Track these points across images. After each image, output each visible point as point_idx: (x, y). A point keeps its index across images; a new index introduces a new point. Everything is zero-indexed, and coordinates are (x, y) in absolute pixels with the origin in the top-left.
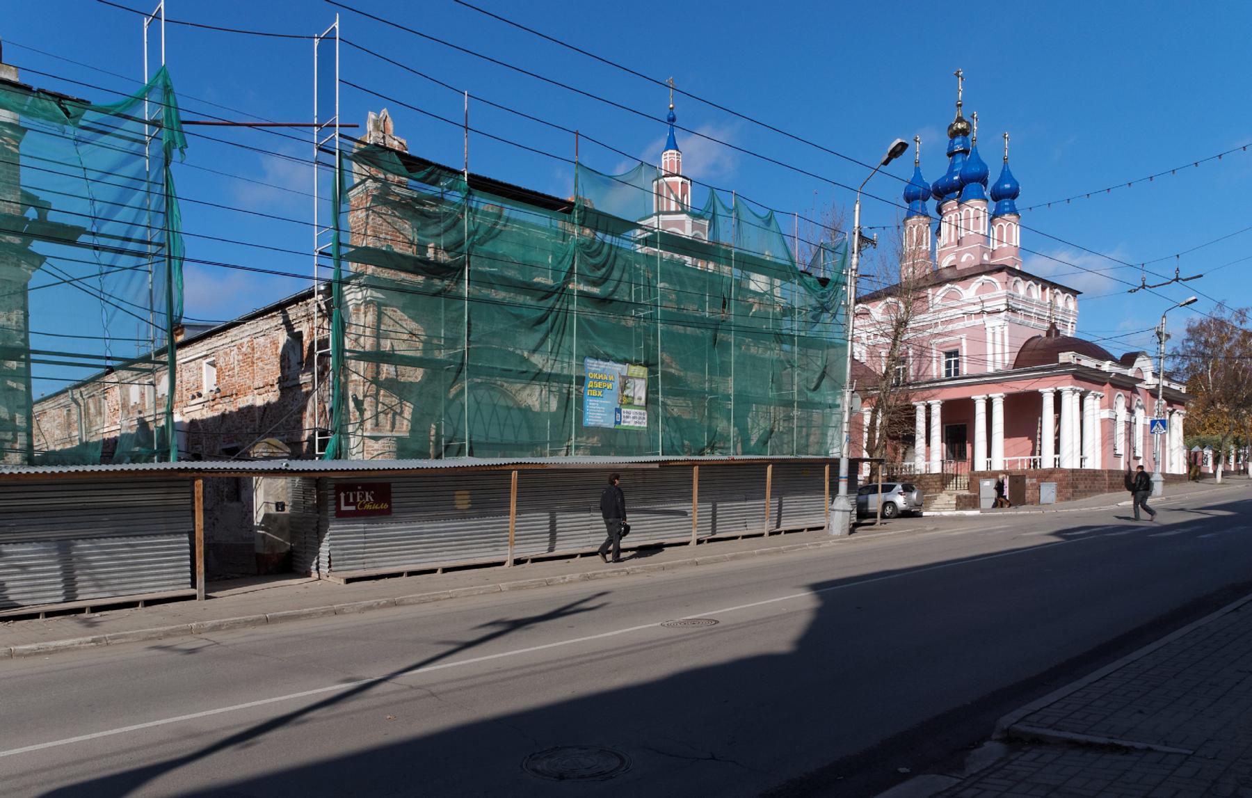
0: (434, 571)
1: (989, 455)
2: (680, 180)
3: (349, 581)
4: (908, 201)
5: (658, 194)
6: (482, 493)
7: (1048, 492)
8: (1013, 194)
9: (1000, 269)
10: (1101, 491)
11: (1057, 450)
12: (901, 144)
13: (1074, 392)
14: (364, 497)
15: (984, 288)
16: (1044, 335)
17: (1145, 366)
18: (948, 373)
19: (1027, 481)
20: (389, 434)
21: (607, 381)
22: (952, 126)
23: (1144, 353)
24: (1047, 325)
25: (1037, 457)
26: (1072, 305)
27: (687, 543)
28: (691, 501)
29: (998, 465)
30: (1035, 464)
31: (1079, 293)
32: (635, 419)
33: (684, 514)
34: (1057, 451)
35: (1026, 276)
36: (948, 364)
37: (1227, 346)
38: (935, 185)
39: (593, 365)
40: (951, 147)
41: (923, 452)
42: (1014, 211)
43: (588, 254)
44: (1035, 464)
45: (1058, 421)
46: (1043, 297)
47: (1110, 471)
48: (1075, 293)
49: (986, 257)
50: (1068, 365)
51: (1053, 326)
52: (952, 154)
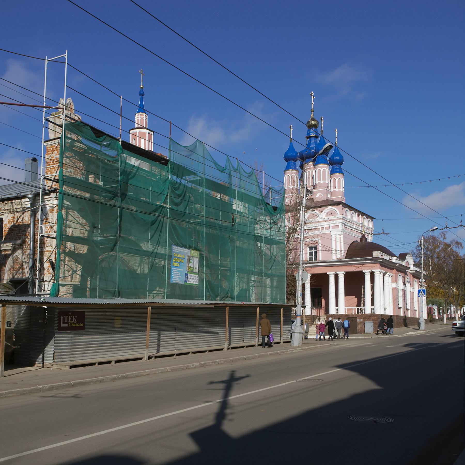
0: (110, 362)
1: (337, 305)
2: (147, 131)
3: (71, 367)
4: (287, 161)
5: (149, 141)
6: (127, 319)
7: (369, 327)
8: (340, 162)
9: (338, 203)
11: (373, 304)
12: (330, 146)
13: (381, 272)
14: (72, 319)
15: (331, 214)
16: (359, 241)
17: (410, 260)
18: (311, 259)
19: (358, 320)
20: (70, 283)
21: (182, 258)
22: (309, 122)
23: (409, 254)
24: (360, 235)
25: (362, 307)
27: (222, 349)
28: (225, 327)
29: (342, 311)
30: (362, 311)
32: (193, 280)
33: (217, 333)
34: (373, 304)
35: (351, 208)
36: (311, 254)
37: (437, 250)
38: (301, 153)
39: (176, 249)
40: (308, 134)
42: (341, 172)
43: (174, 188)
44: (362, 311)
45: (373, 288)
46: (359, 219)
48: (372, 218)
49: (329, 196)
50: (377, 258)
51: (364, 235)
52: (309, 137)
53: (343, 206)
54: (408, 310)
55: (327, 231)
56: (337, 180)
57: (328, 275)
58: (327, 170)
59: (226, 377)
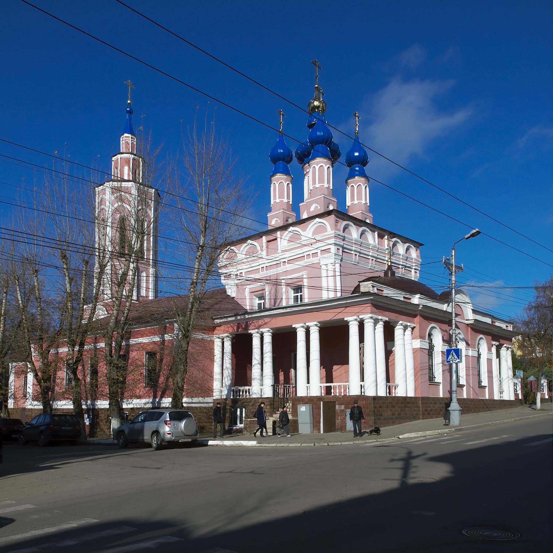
8: (363, 161)
10: (415, 418)
16: (382, 275)
19: (337, 407)
24: (386, 268)
26: (414, 253)
31: (421, 245)
41: (259, 377)
42: (362, 174)
47: (423, 398)
53: (337, 217)
54: (462, 386)
55: (315, 260)
56: (355, 187)
57: (295, 329)
58: (326, 168)
59: (403, 454)
